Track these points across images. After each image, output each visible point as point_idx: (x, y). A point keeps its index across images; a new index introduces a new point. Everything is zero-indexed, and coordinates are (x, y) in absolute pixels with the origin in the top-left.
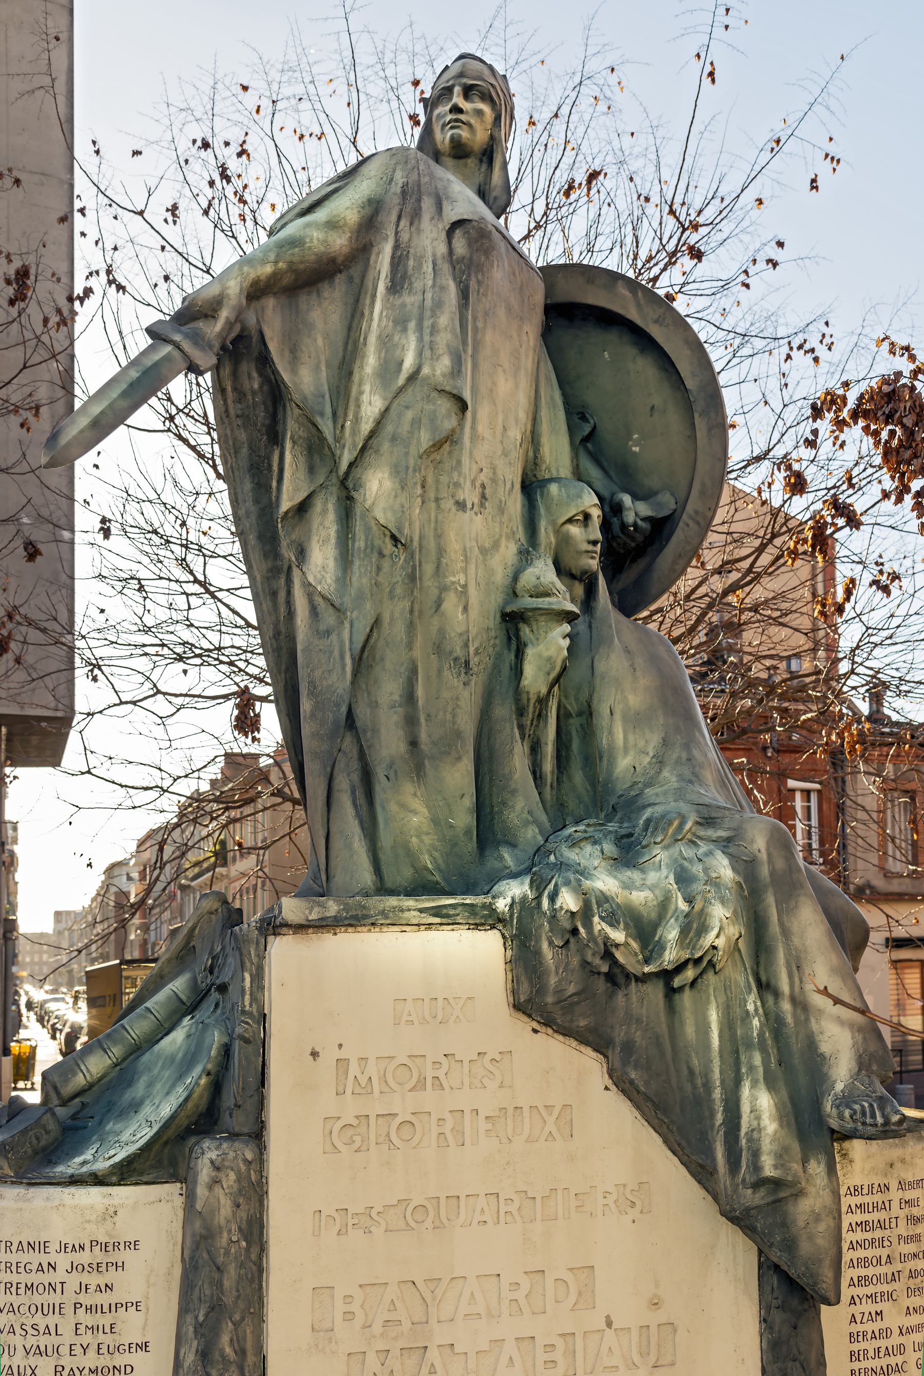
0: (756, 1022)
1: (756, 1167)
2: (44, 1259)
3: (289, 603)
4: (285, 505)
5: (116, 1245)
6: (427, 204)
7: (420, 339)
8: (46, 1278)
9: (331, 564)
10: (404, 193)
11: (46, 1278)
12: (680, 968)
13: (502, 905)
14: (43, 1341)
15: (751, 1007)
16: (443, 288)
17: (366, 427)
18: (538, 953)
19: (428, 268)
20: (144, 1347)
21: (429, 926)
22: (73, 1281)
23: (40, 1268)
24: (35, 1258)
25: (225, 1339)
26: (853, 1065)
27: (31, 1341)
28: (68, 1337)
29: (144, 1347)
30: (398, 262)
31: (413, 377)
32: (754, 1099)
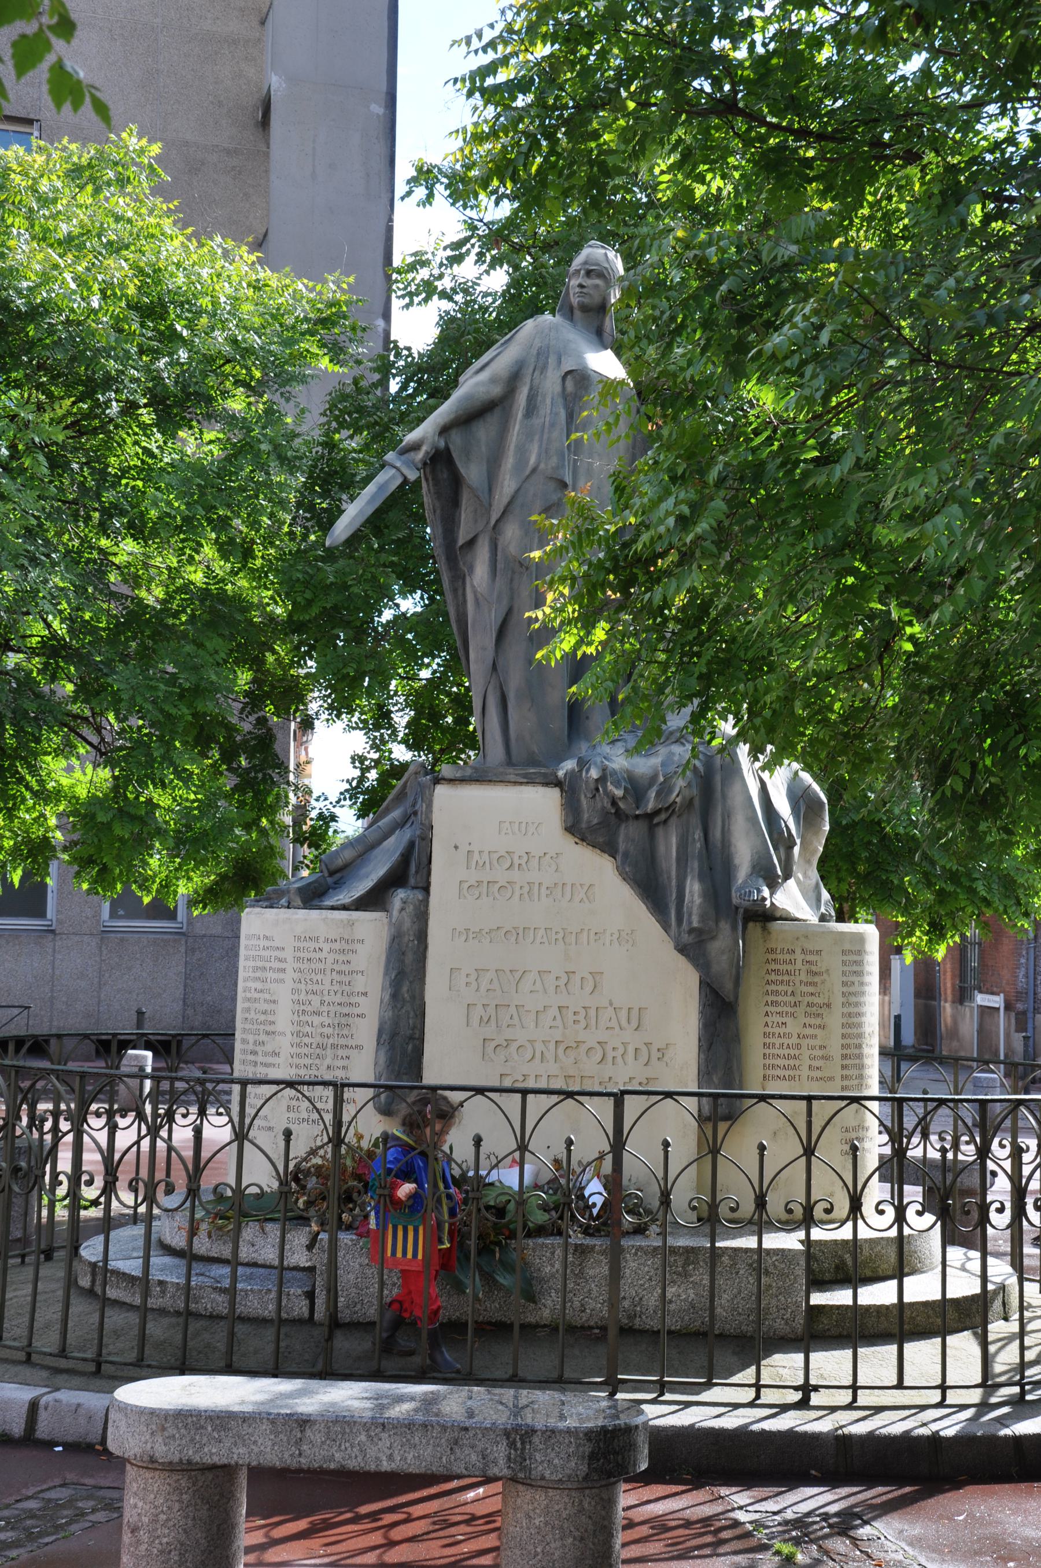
0: (698, 845)
1: (690, 922)
2: (317, 946)
3: (464, 595)
4: (461, 542)
5: (353, 941)
6: (552, 360)
7: (540, 447)
8: (318, 955)
9: (486, 576)
10: (538, 354)
11: (318, 955)
12: (657, 812)
13: (561, 774)
14: (315, 987)
15: (696, 837)
16: (557, 414)
17: (505, 500)
18: (579, 801)
19: (548, 401)
20: (365, 994)
21: (521, 783)
22: (331, 958)
23: (315, 950)
24: (312, 945)
25: (405, 989)
26: (749, 870)
27: (310, 987)
28: (327, 986)
29: (365, 994)
30: (532, 399)
31: (534, 470)
32: (692, 885)
